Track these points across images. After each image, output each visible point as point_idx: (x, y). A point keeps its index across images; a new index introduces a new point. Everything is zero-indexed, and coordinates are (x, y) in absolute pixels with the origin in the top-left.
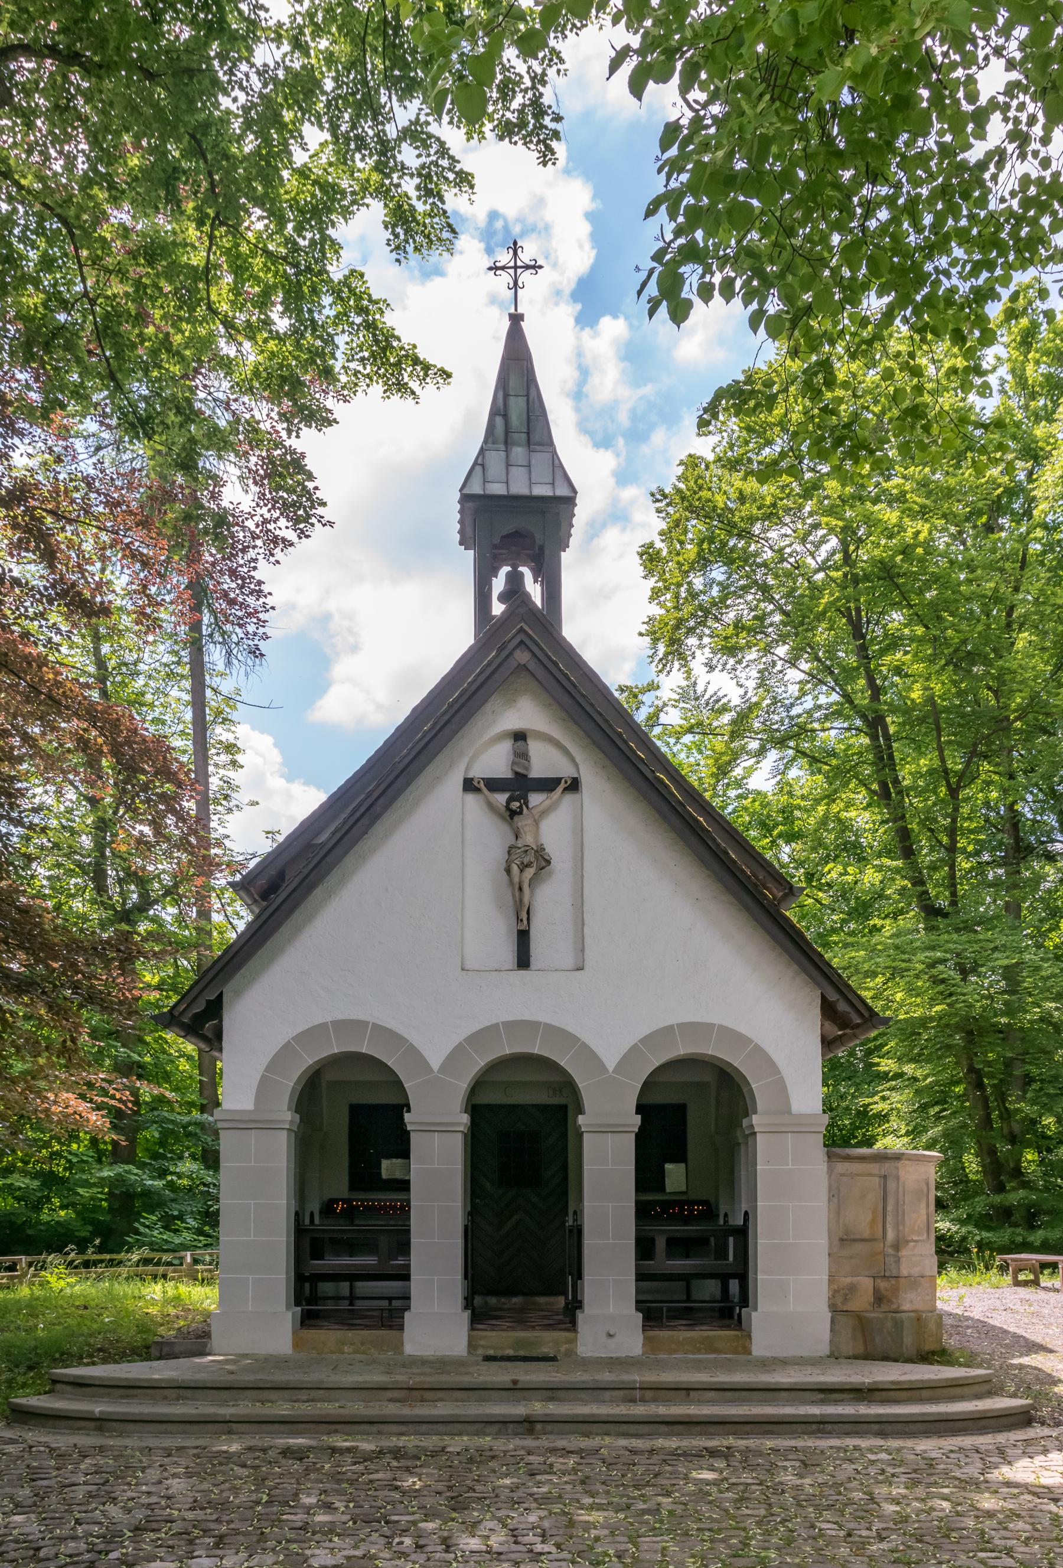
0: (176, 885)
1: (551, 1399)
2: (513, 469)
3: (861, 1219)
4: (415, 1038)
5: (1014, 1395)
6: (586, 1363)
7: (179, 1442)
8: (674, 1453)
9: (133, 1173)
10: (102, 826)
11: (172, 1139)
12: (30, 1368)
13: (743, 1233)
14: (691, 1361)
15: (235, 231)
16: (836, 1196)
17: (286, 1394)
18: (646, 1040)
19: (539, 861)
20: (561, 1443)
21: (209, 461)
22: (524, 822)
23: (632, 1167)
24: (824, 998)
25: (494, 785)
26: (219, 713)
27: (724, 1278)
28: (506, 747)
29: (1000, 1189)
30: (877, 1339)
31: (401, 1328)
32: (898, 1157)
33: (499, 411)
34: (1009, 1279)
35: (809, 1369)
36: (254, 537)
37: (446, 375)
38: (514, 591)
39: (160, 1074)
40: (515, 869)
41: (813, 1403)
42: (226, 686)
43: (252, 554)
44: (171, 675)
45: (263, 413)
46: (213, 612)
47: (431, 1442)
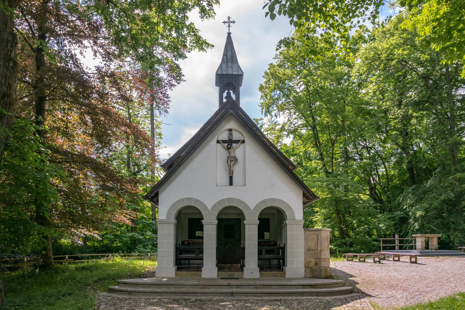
0: (146, 166)
1: (238, 288)
2: (228, 68)
3: (312, 245)
4: (205, 202)
5: (348, 286)
6: (246, 279)
7: (149, 297)
8: (267, 300)
9: (135, 235)
10: (130, 152)
11: (146, 226)
12: (113, 280)
13: (284, 249)
14: (271, 279)
15: (164, 14)
16: (306, 239)
17: (174, 286)
18: (261, 202)
19: (235, 160)
20: (240, 298)
21: (156, 66)
22: (231, 150)
24: (303, 192)
25: (224, 142)
26: (157, 126)
27: (279, 259)
28: (227, 133)
29: (344, 238)
30: (316, 274)
31: (201, 271)
32: (321, 230)
33: (225, 54)
34: (346, 259)
35: (300, 281)
36: (167, 84)
37: (213, 46)
38: (228, 96)
39: (142, 211)
40: (229, 162)
41: (301, 288)
42: (159, 120)
43: (166, 88)
44: (146, 117)
45: (168, 55)
46: (156, 102)
47: (209, 298)
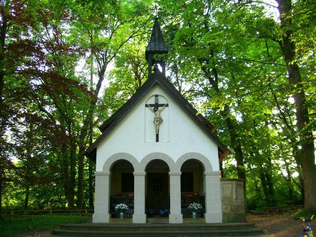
23: (171, 199)
25: (151, 105)
31: (132, 217)
